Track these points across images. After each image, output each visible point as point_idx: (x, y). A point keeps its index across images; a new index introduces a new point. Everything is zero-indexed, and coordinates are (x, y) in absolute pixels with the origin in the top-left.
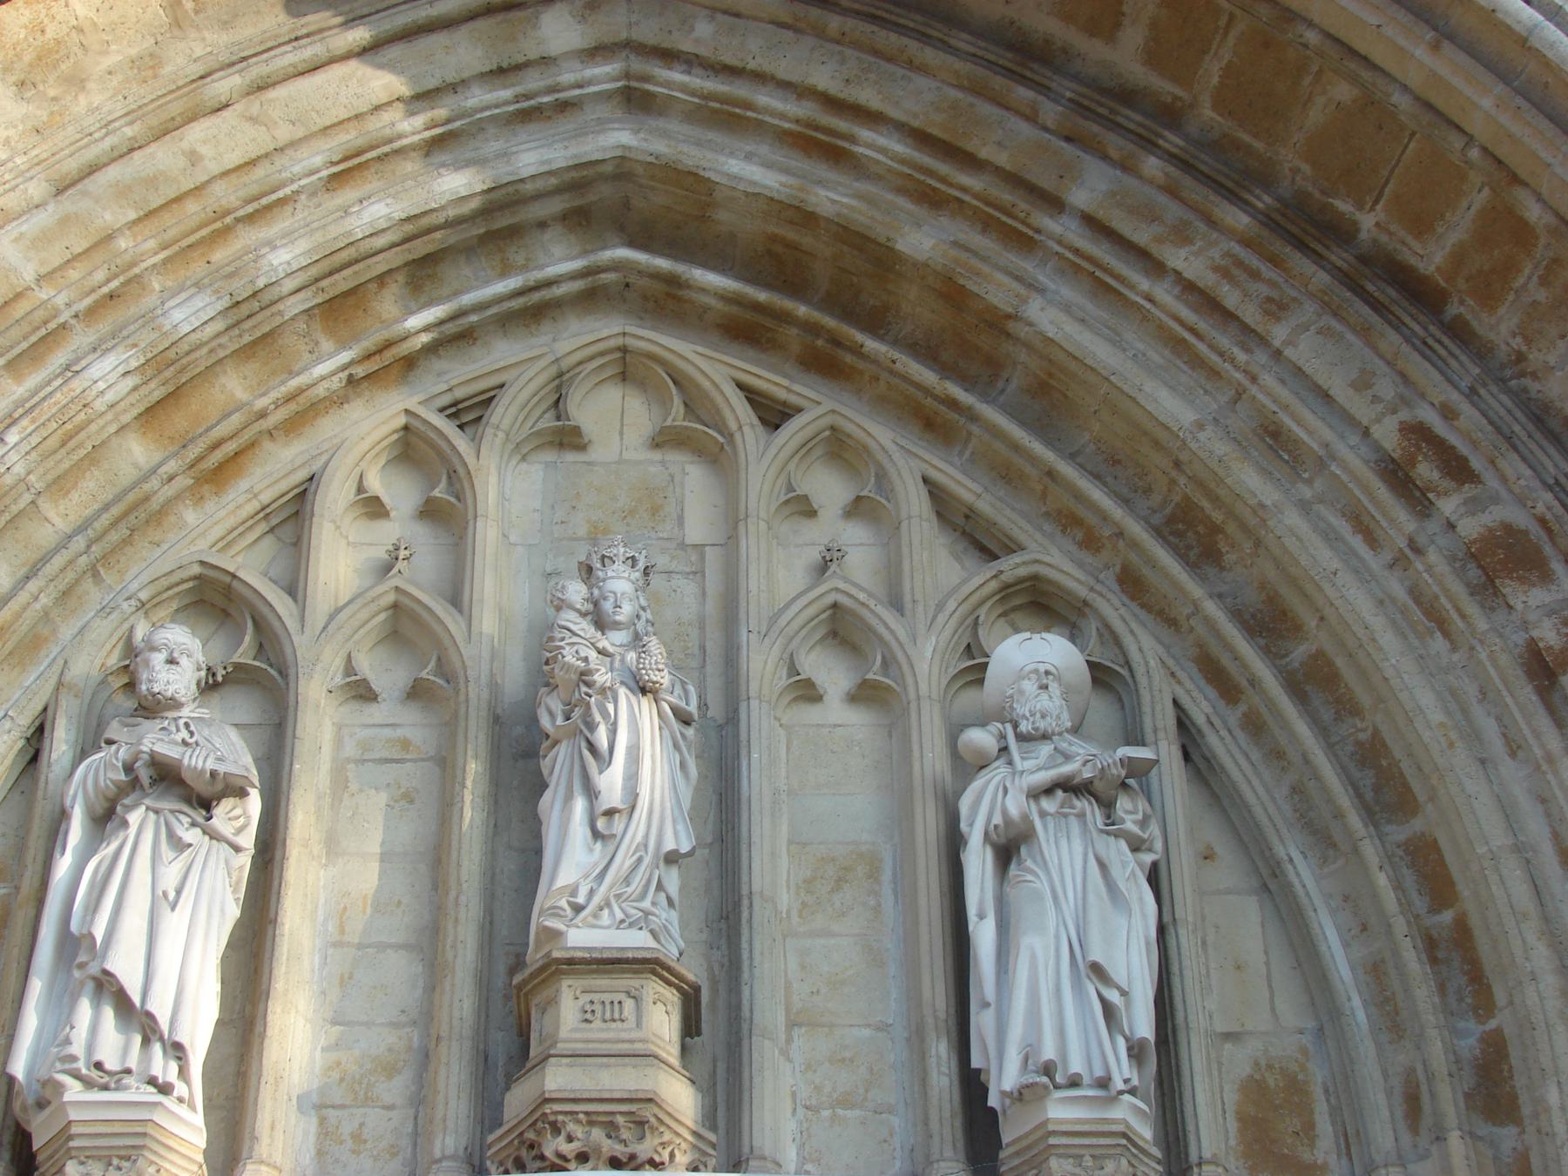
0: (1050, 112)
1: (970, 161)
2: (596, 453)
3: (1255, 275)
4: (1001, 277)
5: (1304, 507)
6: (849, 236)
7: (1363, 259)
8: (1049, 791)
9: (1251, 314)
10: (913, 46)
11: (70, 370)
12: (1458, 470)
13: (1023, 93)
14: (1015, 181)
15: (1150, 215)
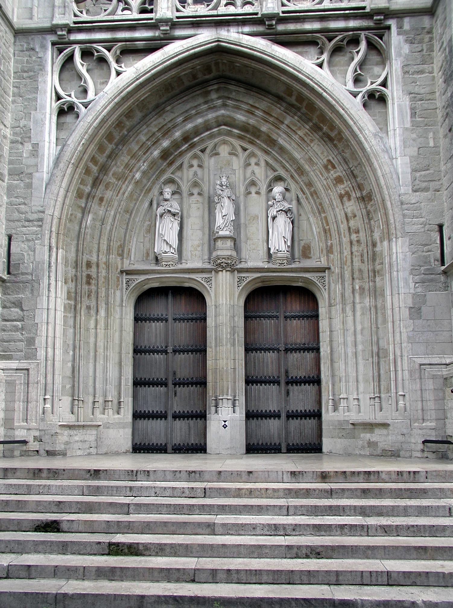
0: (282, 108)
1: (271, 116)
2: (221, 155)
3: (309, 135)
4: (275, 134)
5: (314, 171)
6: (254, 127)
7: (324, 134)
8: (279, 211)
9: (308, 142)
10: (263, 97)
11: (152, 153)
12: (334, 167)
13: (279, 106)
14: (277, 119)
15: (295, 125)
